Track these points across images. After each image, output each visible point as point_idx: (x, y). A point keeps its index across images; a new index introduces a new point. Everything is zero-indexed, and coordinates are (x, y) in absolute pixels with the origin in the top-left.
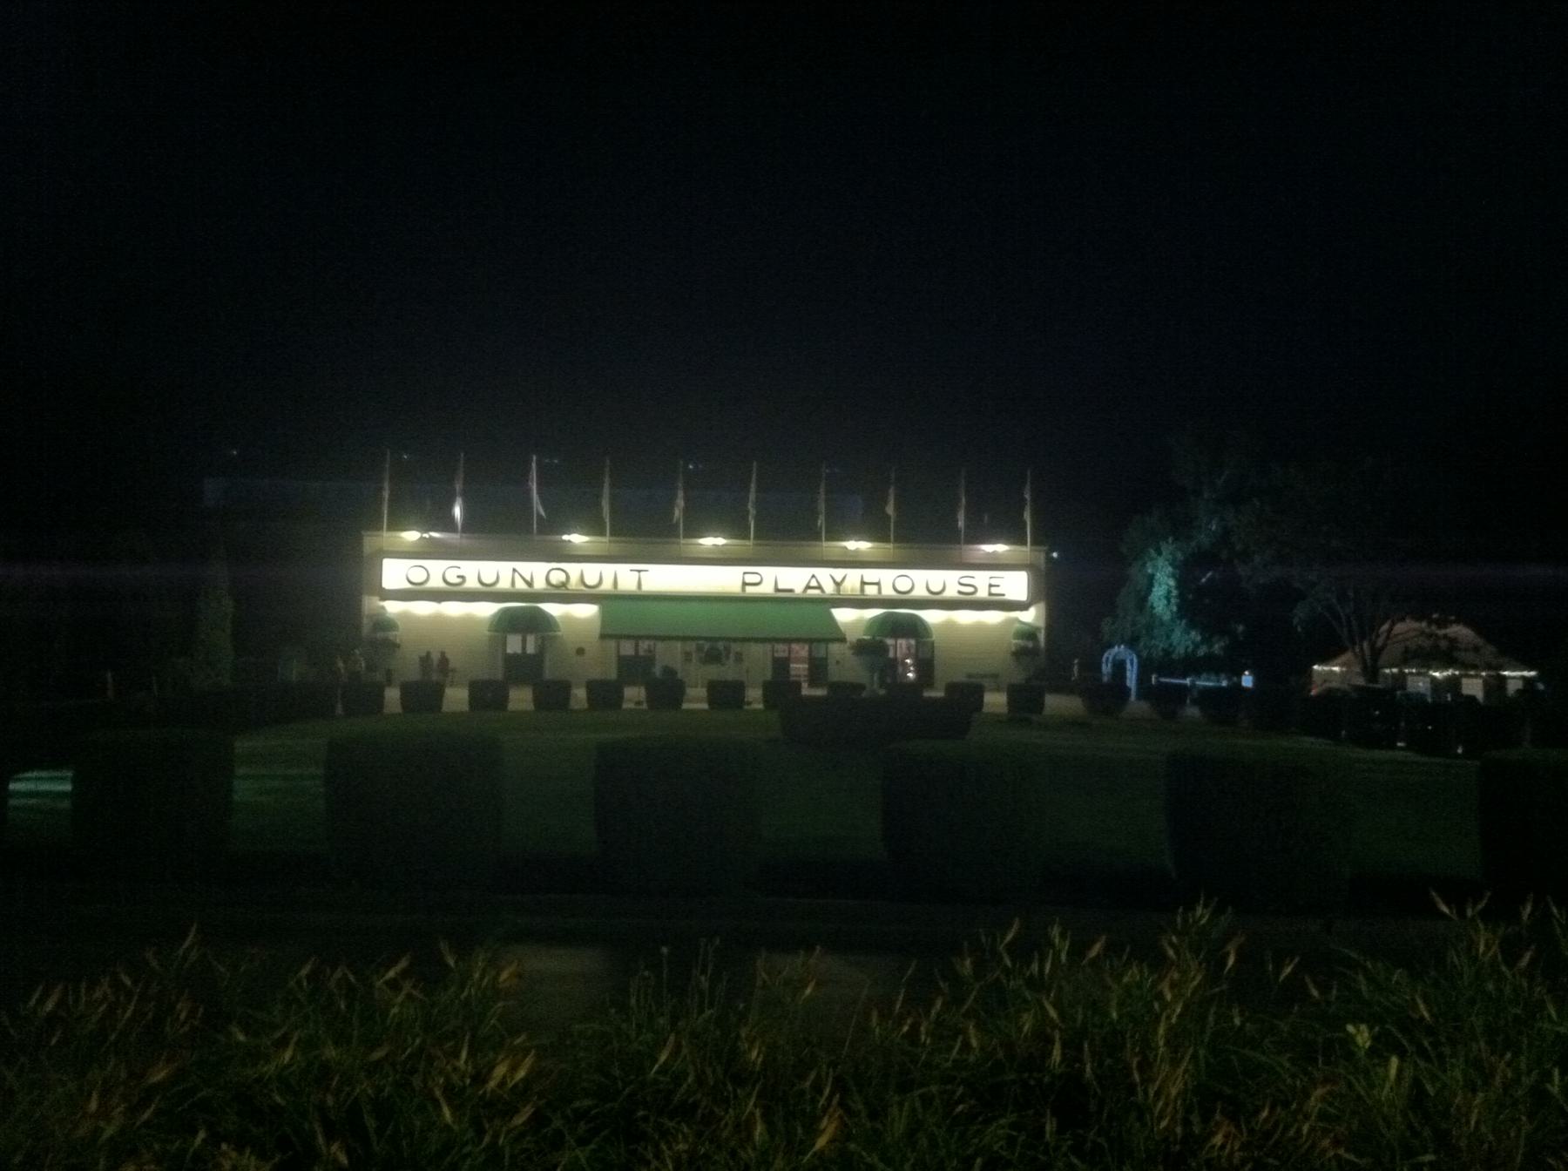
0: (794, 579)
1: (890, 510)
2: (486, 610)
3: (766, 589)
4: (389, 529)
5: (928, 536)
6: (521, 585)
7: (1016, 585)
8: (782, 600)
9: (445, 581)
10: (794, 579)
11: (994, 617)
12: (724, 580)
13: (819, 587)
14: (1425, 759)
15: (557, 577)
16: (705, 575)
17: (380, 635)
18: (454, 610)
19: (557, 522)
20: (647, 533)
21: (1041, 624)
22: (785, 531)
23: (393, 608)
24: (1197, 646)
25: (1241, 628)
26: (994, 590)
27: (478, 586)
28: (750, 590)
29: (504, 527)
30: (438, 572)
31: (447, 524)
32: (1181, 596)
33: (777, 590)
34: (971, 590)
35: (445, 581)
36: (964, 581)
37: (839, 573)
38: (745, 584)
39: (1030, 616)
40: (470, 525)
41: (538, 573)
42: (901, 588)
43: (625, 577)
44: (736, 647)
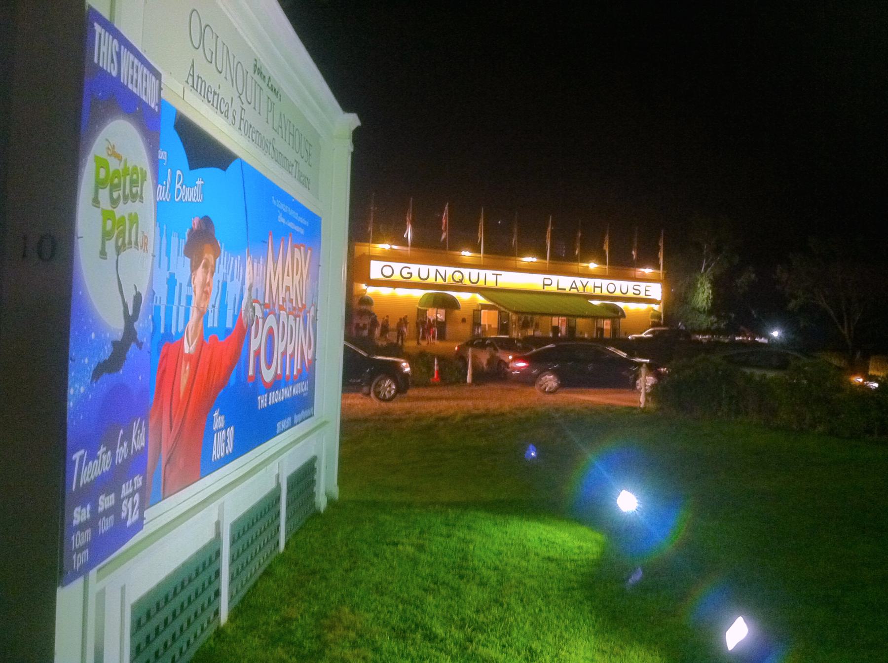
0: (564, 283)
1: (606, 247)
2: (418, 294)
3: (553, 288)
4: (373, 242)
5: (621, 265)
6: (440, 281)
7: (656, 291)
8: (561, 294)
9: (454, 280)
10: (564, 283)
11: (643, 307)
12: (533, 282)
13: (576, 288)
14: (222, 251)
15: (458, 276)
16: (525, 279)
17: (363, 307)
18: (401, 293)
19: (455, 244)
20: (500, 253)
21: (661, 311)
22: (562, 259)
23: (371, 291)
24: (712, 324)
25: (733, 315)
26: (647, 293)
27: (452, 281)
28: (547, 289)
29: (431, 247)
30: (397, 270)
31: (403, 242)
32: (714, 299)
33: (558, 289)
34: (637, 292)
35: (454, 280)
36: (636, 287)
37: (585, 280)
38: (544, 285)
39: (656, 307)
40: (416, 244)
41: (448, 273)
42: (457, 280)
43: (489, 278)
44: (536, 318)
